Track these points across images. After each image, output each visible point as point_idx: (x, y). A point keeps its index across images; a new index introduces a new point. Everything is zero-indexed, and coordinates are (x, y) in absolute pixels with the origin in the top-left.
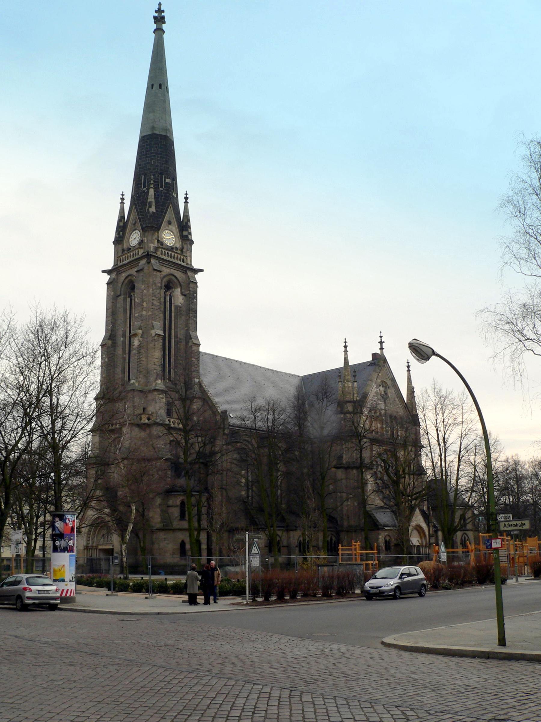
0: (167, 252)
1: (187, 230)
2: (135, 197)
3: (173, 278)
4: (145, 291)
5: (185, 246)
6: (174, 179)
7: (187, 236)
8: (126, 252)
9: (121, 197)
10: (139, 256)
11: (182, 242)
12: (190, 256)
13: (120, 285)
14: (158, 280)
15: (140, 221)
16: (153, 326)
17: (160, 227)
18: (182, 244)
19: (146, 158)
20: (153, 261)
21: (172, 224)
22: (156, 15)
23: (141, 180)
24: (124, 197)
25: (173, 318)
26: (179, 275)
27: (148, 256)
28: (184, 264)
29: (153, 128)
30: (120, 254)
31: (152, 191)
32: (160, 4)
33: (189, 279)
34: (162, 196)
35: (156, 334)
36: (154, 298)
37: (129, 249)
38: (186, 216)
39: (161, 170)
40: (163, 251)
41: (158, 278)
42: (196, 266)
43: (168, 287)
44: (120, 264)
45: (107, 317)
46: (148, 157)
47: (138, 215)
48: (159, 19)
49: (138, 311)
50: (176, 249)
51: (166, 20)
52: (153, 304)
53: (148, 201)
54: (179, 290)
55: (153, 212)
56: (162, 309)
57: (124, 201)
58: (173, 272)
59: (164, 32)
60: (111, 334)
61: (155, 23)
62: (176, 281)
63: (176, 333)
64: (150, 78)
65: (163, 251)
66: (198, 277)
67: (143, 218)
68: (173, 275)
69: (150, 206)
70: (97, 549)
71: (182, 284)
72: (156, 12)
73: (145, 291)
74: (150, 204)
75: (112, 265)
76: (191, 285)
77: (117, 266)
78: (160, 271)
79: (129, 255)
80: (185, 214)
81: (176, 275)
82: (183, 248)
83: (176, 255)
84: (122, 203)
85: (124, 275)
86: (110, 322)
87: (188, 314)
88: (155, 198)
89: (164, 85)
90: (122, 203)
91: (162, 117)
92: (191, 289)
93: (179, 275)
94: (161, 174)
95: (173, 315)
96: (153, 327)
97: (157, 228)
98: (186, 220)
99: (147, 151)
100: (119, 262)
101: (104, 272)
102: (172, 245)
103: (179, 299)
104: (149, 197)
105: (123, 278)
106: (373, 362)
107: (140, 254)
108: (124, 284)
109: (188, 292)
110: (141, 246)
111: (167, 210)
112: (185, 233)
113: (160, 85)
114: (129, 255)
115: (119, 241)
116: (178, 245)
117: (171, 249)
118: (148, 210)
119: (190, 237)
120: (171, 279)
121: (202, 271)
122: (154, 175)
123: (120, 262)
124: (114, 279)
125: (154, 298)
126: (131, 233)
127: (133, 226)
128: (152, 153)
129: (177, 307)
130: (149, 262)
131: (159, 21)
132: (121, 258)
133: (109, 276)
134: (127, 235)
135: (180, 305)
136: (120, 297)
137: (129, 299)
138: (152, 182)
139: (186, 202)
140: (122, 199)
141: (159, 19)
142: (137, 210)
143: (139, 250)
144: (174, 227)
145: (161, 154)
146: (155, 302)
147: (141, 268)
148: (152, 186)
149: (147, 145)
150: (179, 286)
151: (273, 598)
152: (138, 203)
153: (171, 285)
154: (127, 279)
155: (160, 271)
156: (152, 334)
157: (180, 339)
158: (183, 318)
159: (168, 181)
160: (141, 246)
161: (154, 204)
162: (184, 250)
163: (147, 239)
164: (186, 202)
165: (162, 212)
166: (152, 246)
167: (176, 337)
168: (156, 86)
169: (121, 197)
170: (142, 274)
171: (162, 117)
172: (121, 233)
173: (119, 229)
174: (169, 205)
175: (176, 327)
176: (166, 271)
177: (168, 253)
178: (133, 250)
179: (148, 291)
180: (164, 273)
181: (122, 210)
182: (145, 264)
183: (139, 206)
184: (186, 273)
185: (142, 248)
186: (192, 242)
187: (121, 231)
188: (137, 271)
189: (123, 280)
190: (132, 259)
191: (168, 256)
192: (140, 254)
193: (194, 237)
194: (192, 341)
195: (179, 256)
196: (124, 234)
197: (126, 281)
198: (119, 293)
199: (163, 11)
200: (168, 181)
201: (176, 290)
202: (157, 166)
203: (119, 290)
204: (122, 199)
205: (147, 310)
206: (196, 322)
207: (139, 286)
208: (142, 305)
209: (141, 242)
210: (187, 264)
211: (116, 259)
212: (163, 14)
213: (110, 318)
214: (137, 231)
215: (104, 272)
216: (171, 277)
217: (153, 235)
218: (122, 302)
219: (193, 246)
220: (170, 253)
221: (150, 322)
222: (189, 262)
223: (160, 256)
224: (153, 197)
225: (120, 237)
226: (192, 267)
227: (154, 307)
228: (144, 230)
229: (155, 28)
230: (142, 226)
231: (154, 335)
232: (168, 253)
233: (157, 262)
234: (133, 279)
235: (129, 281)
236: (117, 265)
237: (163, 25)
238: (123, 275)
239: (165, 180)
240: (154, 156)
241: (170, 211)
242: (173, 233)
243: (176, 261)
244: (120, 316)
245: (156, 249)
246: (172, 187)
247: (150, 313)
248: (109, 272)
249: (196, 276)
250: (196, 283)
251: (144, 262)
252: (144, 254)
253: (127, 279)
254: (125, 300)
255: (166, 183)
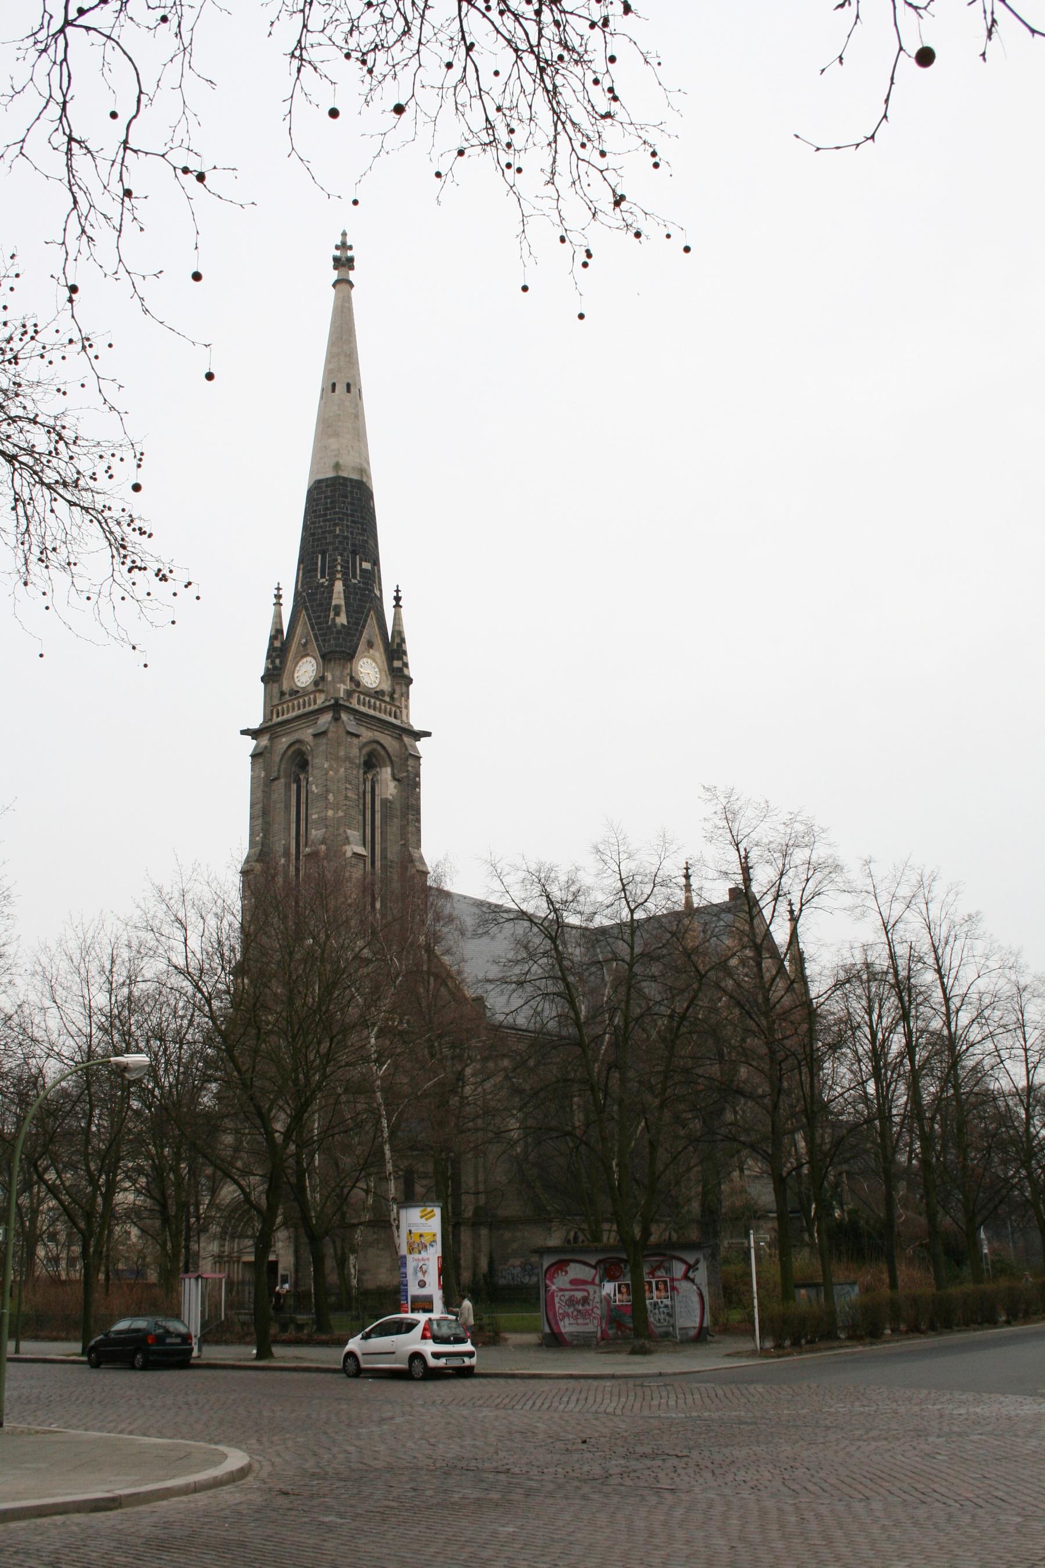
0: (367, 699)
1: (401, 659)
2: (304, 594)
3: (379, 748)
4: (331, 773)
5: (397, 688)
6: (376, 562)
7: (401, 670)
8: (287, 697)
9: (276, 592)
10: (316, 707)
11: (393, 681)
12: (407, 707)
13: (277, 759)
14: (355, 751)
15: (317, 640)
16: (347, 838)
17: (355, 652)
18: (392, 686)
19: (324, 521)
20: (344, 716)
21: (375, 647)
22: (338, 253)
23: (317, 564)
24: (281, 592)
25: (378, 823)
26: (388, 741)
27: (336, 708)
28: (397, 722)
29: (337, 466)
30: (276, 702)
31: (339, 586)
32: (344, 234)
33: (406, 749)
34: (357, 594)
35: (354, 853)
36: (348, 786)
37: (295, 693)
38: (399, 633)
39: (353, 545)
40: (362, 697)
41: (355, 751)
42: (417, 726)
43: (370, 763)
44: (275, 720)
45: (252, 818)
46: (328, 520)
47: (313, 629)
48: (344, 263)
49: (318, 810)
50: (382, 693)
51: (355, 264)
52: (346, 798)
53: (334, 603)
54: (389, 770)
55: (343, 625)
56: (361, 807)
57: (281, 601)
58: (379, 736)
59: (351, 285)
60: (261, 850)
61: (335, 268)
62: (383, 753)
63: (384, 850)
64: (328, 372)
65: (362, 697)
66: (422, 746)
67: (321, 635)
68: (378, 743)
69: (337, 614)
70: (238, 1262)
71: (394, 758)
72: (337, 248)
73: (331, 773)
74: (337, 610)
75: (261, 720)
76: (411, 762)
77: (270, 724)
78: (357, 736)
79: (296, 702)
80: (397, 628)
81: (382, 741)
82: (393, 692)
83: (383, 705)
84: (278, 604)
85: (285, 741)
86: (258, 828)
87: (404, 815)
88: (346, 598)
89: (355, 384)
90: (278, 604)
91: (352, 447)
92: (410, 769)
93: (388, 741)
94: (354, 553)
95: (378, 816)
96: (347, 841)
97: (349, 656)
98: (397, 640)
99: (326, 509)
100: (275, 716)
101: (244, 732)
102: (374, 685)
103: (388, 788)
104: (335, 596)
105: (285, 747)
106: (730, 905)
107: (319, 702)
108: (287, 756)
109: (405, 774)
110: (320, 687)
111: (366, 621)
112: (397, 664)
113: (348, 386)
114: (296, 702)
115: (272, 676)
116: (386, 687)
117: (378, 694)
118: (334, 620)
119: (405, 670)
120: (375, 750)
121: (428, 734)
122: (341, 555)
123: (278, 716)
124: (266, 747)
125: (348, 786)
126: (298, 663)
127: (301, 648)
128: (335, 513)
129: (385, 802)
130: (337, 719)
131: (343, 265)
132: (280, 708)
133: (254, 742)
134: (289, 664)
135: (390, 797)
136: (276, 782)
137: (294, 786)
138: (339, 568)
139: (397, 606)
140: (278, 597)
141: (344, 263)
142: (310, 619)
143: (317, 695)
144: (379, 653)
145: (352, 516)
146: (350, 794)
147: (323, 729)
148: (339, 576)
149: (326, 498)
150: (388, 763)
151: (787, 1343)
152: (312, 607)
153: (374, 760)
154: (292, 749)
155: (357, 736)
156: (345, 853)
157: (391, 862)
158: (396, 821)
159: (366, 566)
160: (320, 687)
161: (344, 609)
162: (396, 696)
163: (333, 675)
164: (397, 606)
165: (357, 624)
166: (342, 688)
167: (384, 857)
168: (341, 388)
169: (276, 592)
170: (324, 741)
171: (352, 447)
172: (277, 661)
173: (274, 654)
174: (369, 611)
175: (384, 840)
176: (367, 734)
177: (386, 708)
178: (305, 695)
179: (337, 772)
180: (363, 740)
181: (278, 616)
182: (330, 723)
183: (314, 612)
184: (400, 739)
185: (321, 691)
186: (410, 681)
187: (278, 656)
188: (315, 736)
189: (283, 751)
190: (301, 711)
191: (369, 707)
192: (319, 702)
193: (413, 672)
194: (415, 866)
195: (372, 701)
196: (283, 662)
197: (290, 752)
198: (275, 775)
199: (350, 248)
200: (366, 566)
201: (384, 769)
202: (346, 538)
203: (276, 769)
204: (278, 597)
205: (336, 807)
206: (418, 830)
207: (319, 763)
208: (327, 799)
209: (319, 681)
210: (402, 722)
211: (269, 709)
212: (350, 253)
213: (260, 821)
214: (309, 659)
215: (244, 732)
216: (375, 746)
217: (344, 667)
218: (282, 791)
219: (411, 687)
220: (372, 701)
221: (341, 831)
222: (404, 718)
223: (357, 707)
224: (342, 596)
225: (275, 668)
226: (406, 726)
227: (348, 803)
228: (326, 658)
229: (335, 278)
230: (320, 650)
231: (349, 854)
232: (386, 708)
233: (352, 718)
234: (304, 749)
235: (294, 753)
236: (271, 720)
237: (351, 272)
238: (284, 740)
239: (361, 565)
240: (340, 519)
241: (372, 621)
242: (376, 663)
243: (383, 716)
244: (279, 817)
245: (349, 694)
246: (372, 578)
247: (341, 814)
248: (254, 734)
249: (417, 743)
250: (419, 758)
251: (326, 718)
252: (327, 704)
253: (292, 749)
254: (288, 787)
255: (362, 570)
